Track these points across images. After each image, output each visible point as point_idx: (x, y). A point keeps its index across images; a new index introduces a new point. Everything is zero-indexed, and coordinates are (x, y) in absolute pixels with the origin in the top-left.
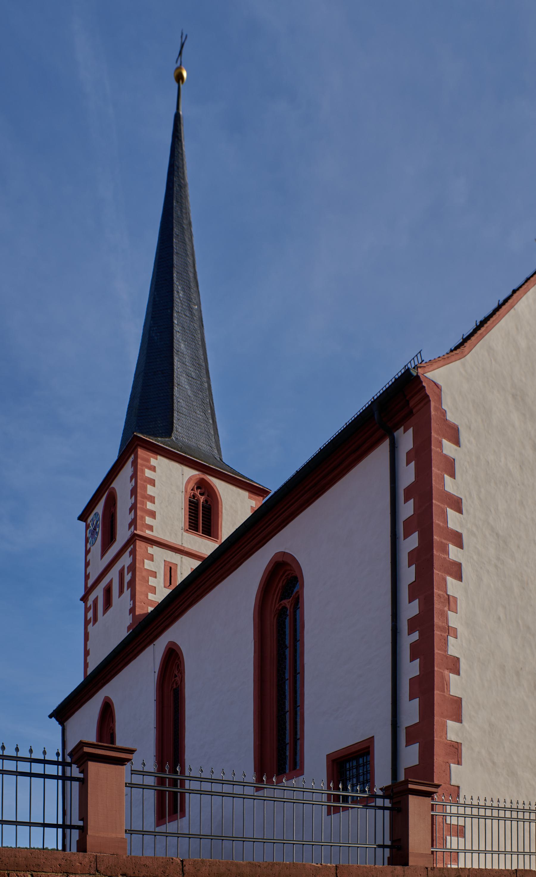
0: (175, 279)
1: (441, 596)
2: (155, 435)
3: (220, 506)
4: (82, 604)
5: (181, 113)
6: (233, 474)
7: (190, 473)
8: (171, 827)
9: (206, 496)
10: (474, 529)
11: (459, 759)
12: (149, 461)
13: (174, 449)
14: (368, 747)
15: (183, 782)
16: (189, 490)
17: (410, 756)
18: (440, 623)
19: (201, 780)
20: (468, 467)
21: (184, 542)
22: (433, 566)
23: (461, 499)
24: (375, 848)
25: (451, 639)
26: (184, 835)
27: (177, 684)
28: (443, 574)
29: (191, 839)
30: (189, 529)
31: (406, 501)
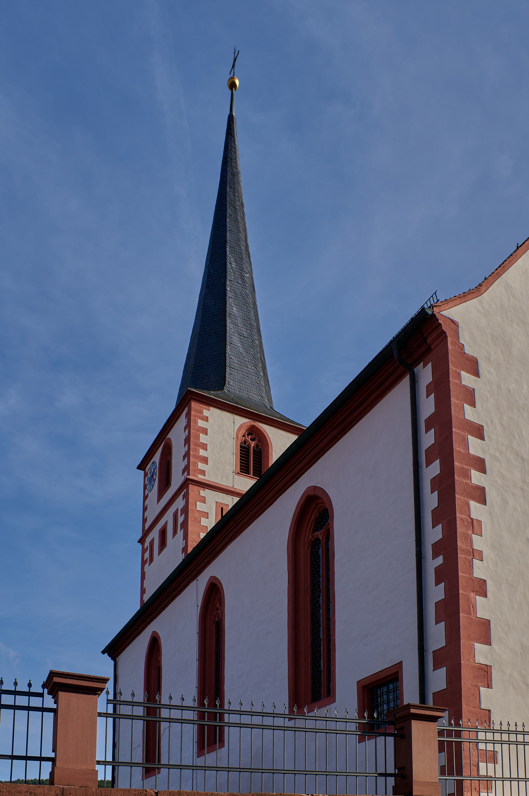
0: (228, 253)
1: (465, 520)
2: (208, 389)
3: (270, 450)
4: (140, 545)
5: (234, 114)
6: (282, 420)
7: (241, 421)
8: (210, 759)
9: (257, 441)
10: (498, 455)
11: (489, 682)
12: (201, 412)
13: (226, 400)
14: (397, 673)
15: (222, 715)
16: (240, 436)
17: (438, 680)
18: (464, 547)
19: (240, 713)
20: (488, 396)
21: (235, 484)
22: (455, 490)
23: (483, 426)
24: (376, 777)
25: (476, 562)
26: (211, 768)
27: (218, 617)
28: (466, 499)
29: (195, 771)
30: (241, 472)
31: (427, 431)
